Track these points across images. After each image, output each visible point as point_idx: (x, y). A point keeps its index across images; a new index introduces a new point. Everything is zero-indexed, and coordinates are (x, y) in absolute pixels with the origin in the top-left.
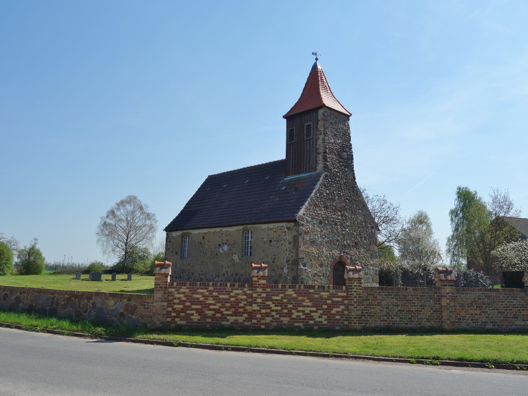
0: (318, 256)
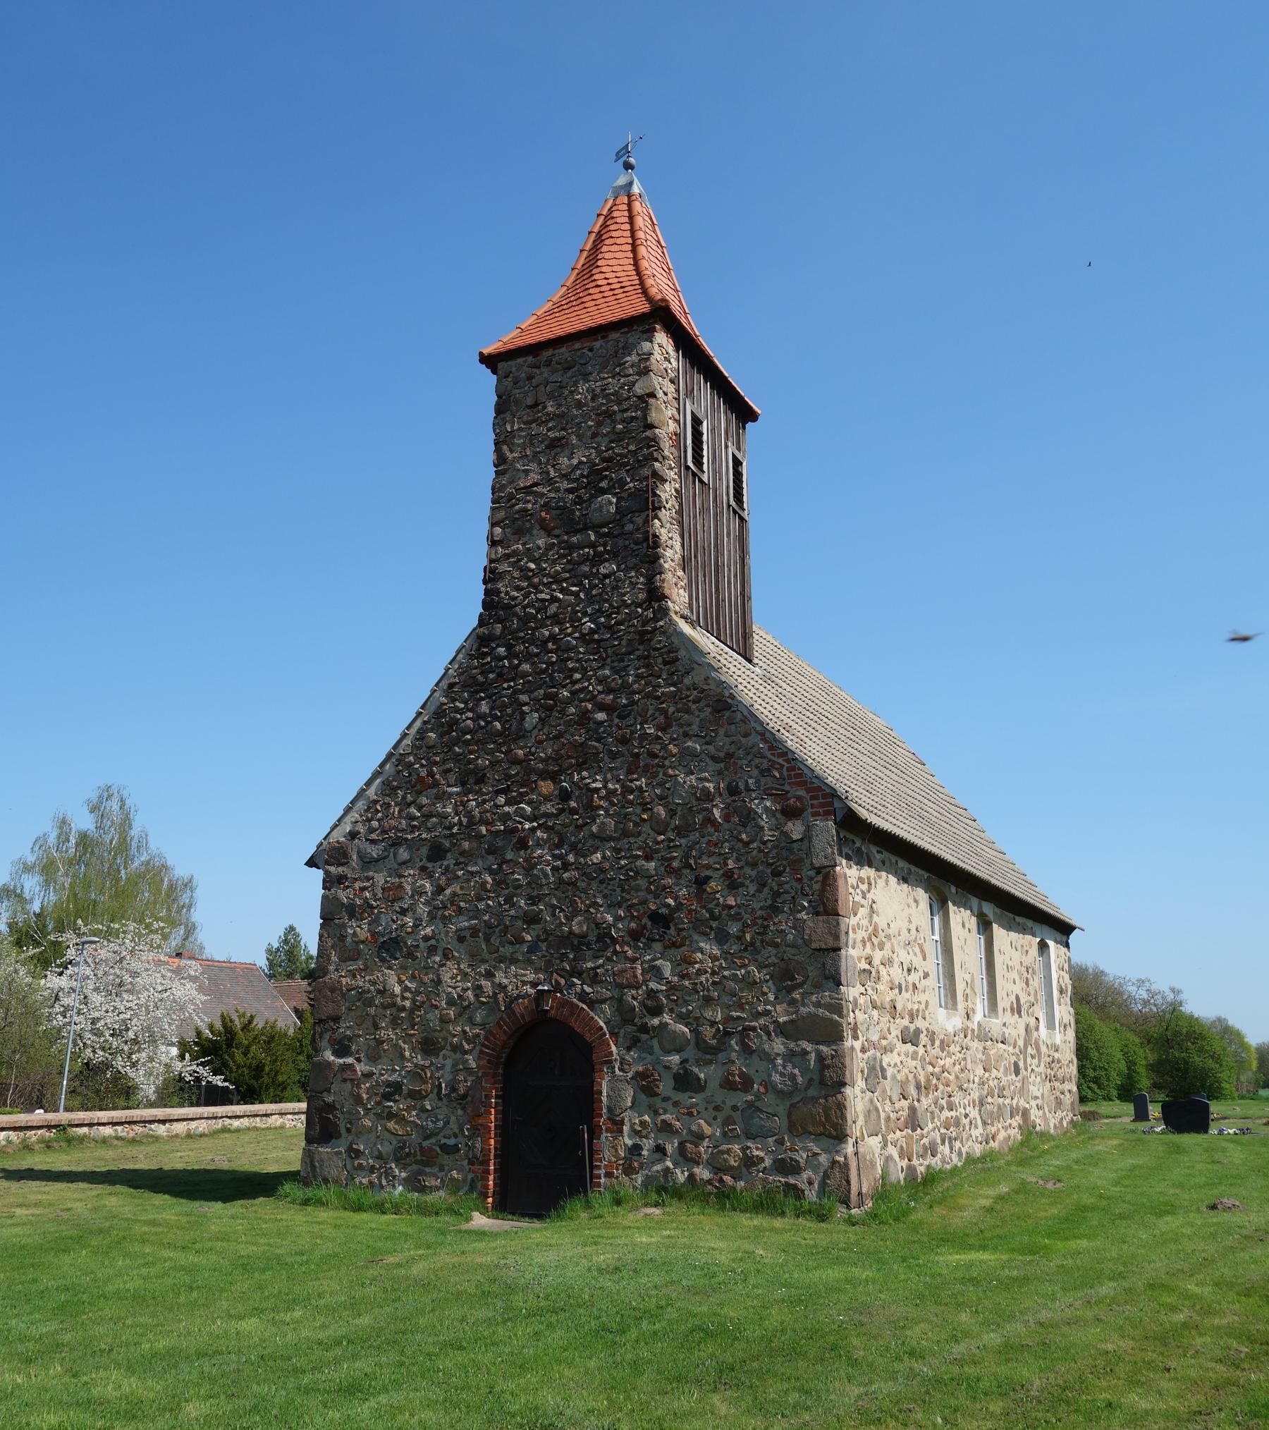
0: (414, 1001)
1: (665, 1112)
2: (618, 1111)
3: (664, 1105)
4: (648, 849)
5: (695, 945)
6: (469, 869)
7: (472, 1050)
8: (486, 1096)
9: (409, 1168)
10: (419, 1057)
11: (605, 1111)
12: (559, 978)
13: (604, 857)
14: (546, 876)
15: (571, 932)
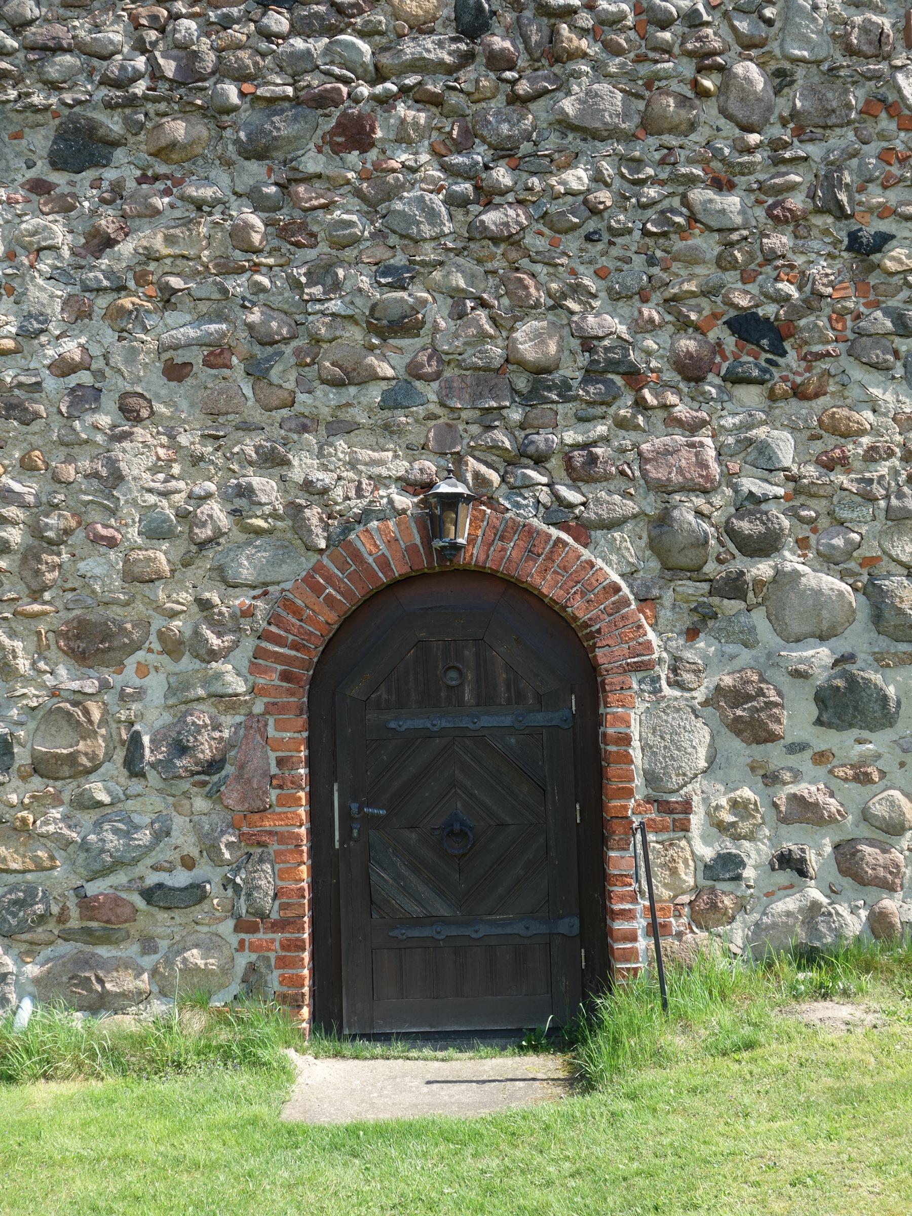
0: (36, 531)
1: (797, 776)
2: (675, 781)
3: (793, 760)
4: (716, 165)
5: (854, 392)
6: (192, 191)
7: (230, 650)
8: (280, 762)
9: (47, 952)
10: (62, 671)
11: (638, 781)
12: (483, 469)
13: (598, 179)
14: (432, 215)
15: (512, 359)
